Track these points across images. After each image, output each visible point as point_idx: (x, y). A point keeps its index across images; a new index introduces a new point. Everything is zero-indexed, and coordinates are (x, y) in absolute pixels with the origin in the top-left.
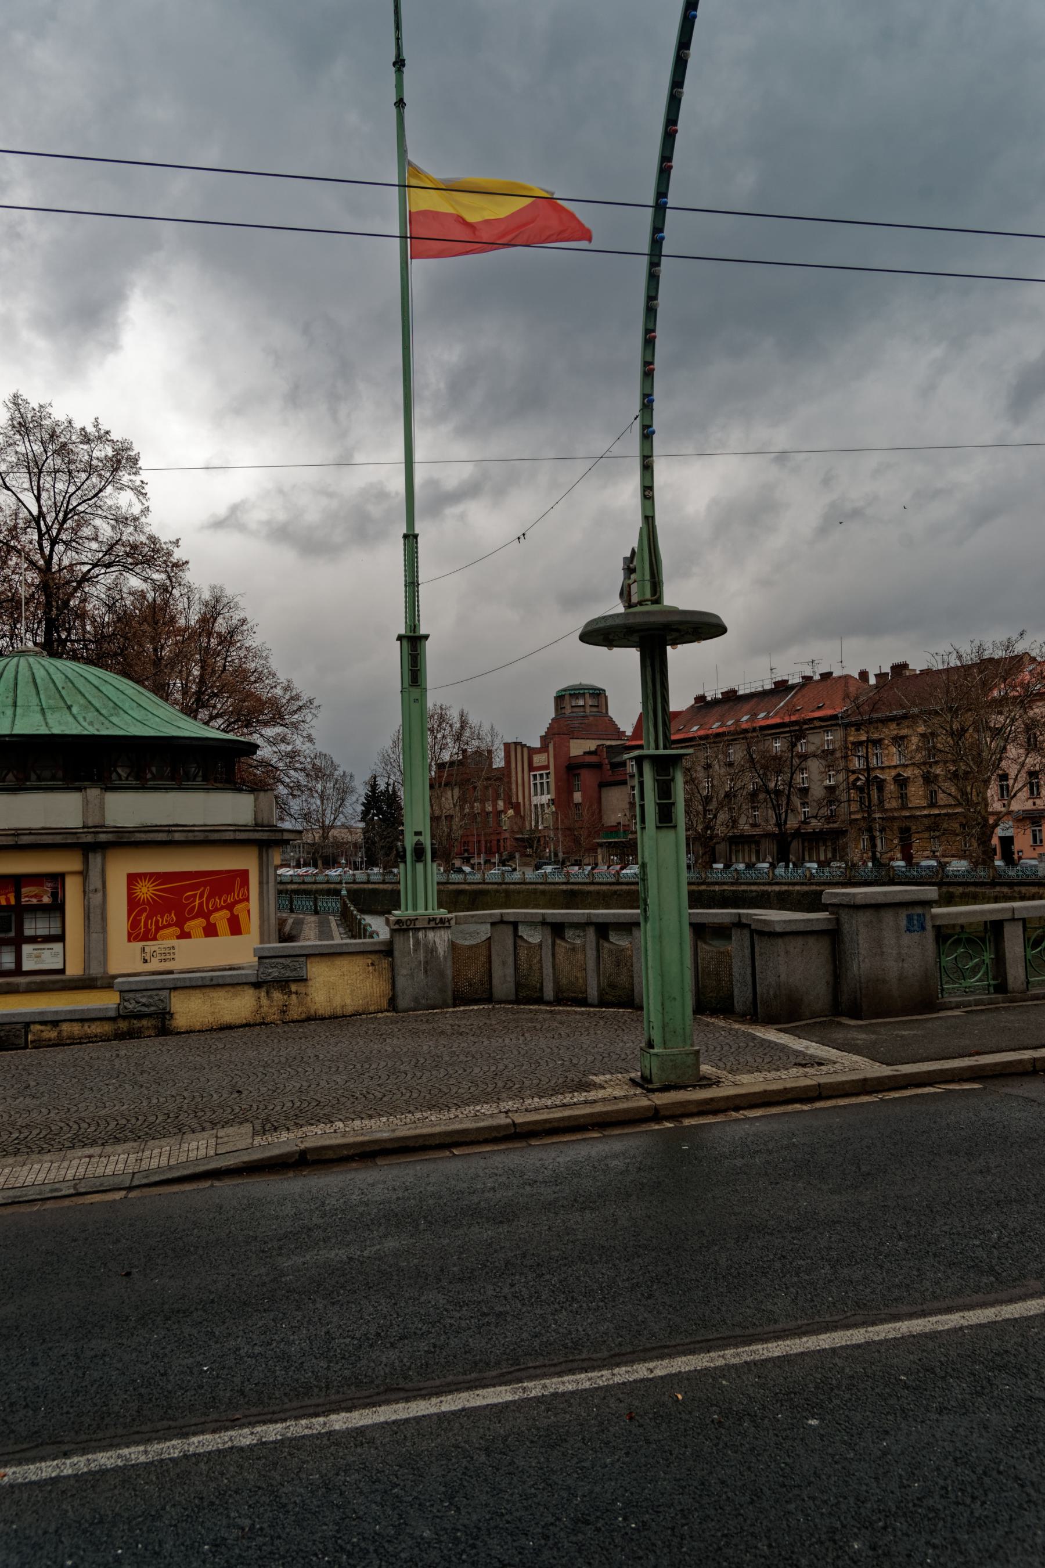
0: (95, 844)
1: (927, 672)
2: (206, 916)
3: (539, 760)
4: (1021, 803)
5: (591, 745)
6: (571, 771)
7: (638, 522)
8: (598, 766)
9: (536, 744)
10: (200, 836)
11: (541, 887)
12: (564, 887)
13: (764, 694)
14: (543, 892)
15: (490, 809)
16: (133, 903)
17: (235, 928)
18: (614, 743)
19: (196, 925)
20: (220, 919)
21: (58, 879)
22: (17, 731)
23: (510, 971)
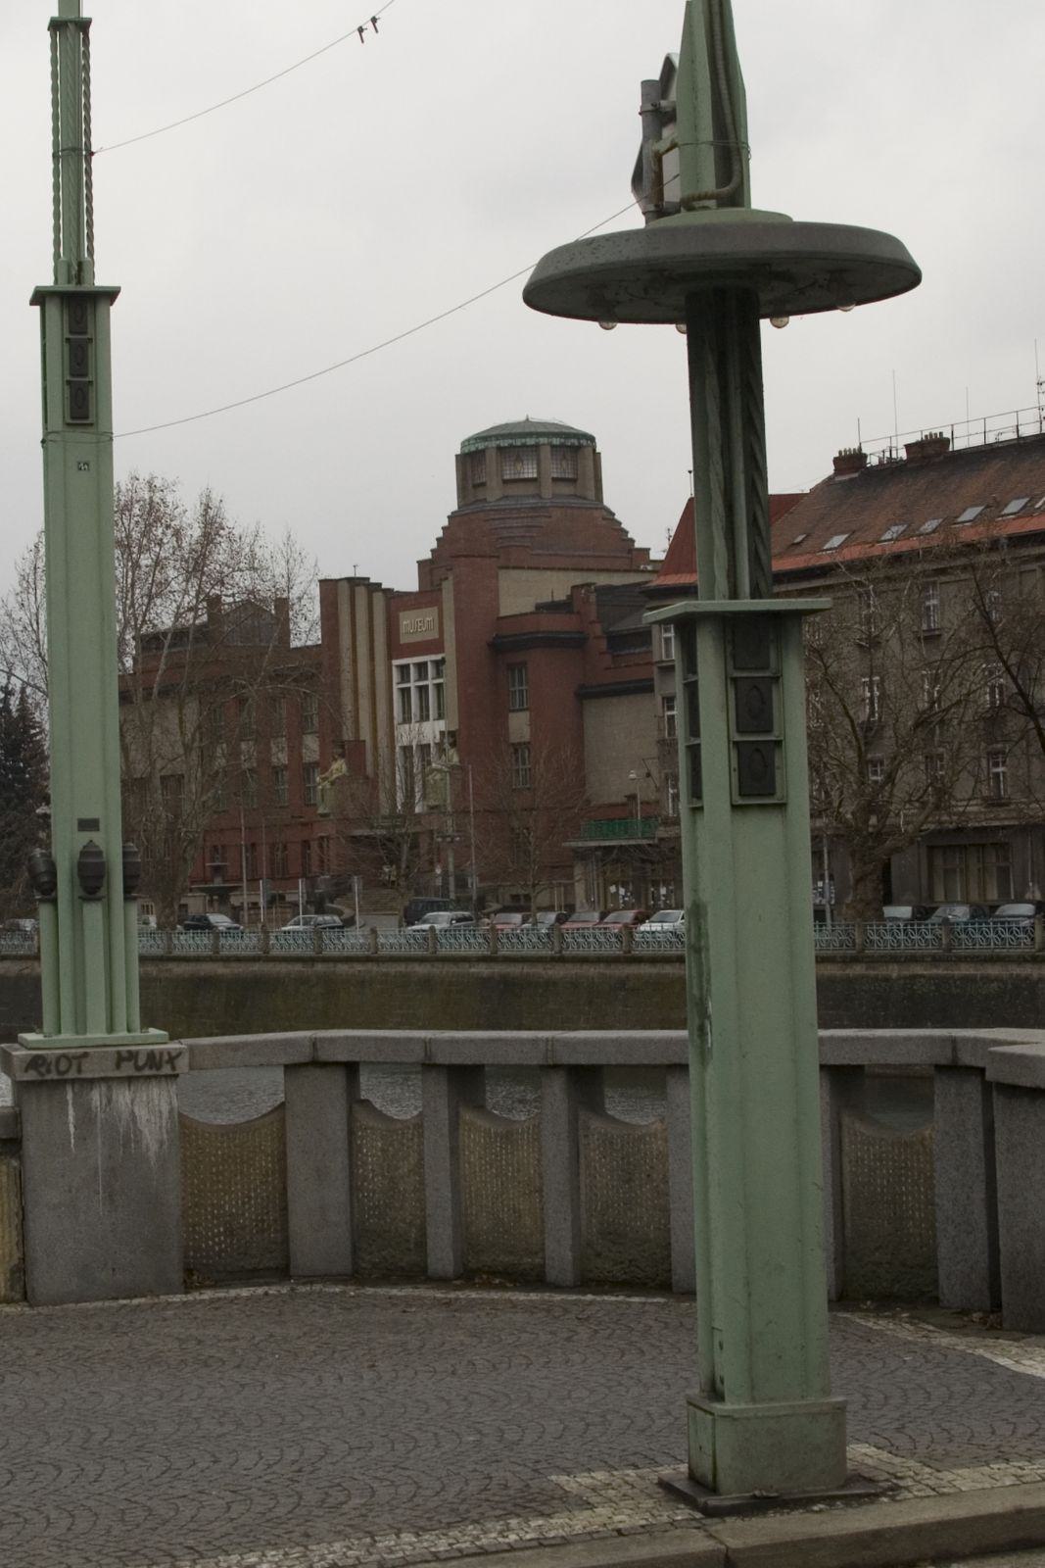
3: (415, 625)
5: (557, 586)
6: (502, 654)
8: (576, 643)
11: (420, 969)
12: (483, 970)
14: (426, 983)
15: (281, 757)
18: (617, 580)
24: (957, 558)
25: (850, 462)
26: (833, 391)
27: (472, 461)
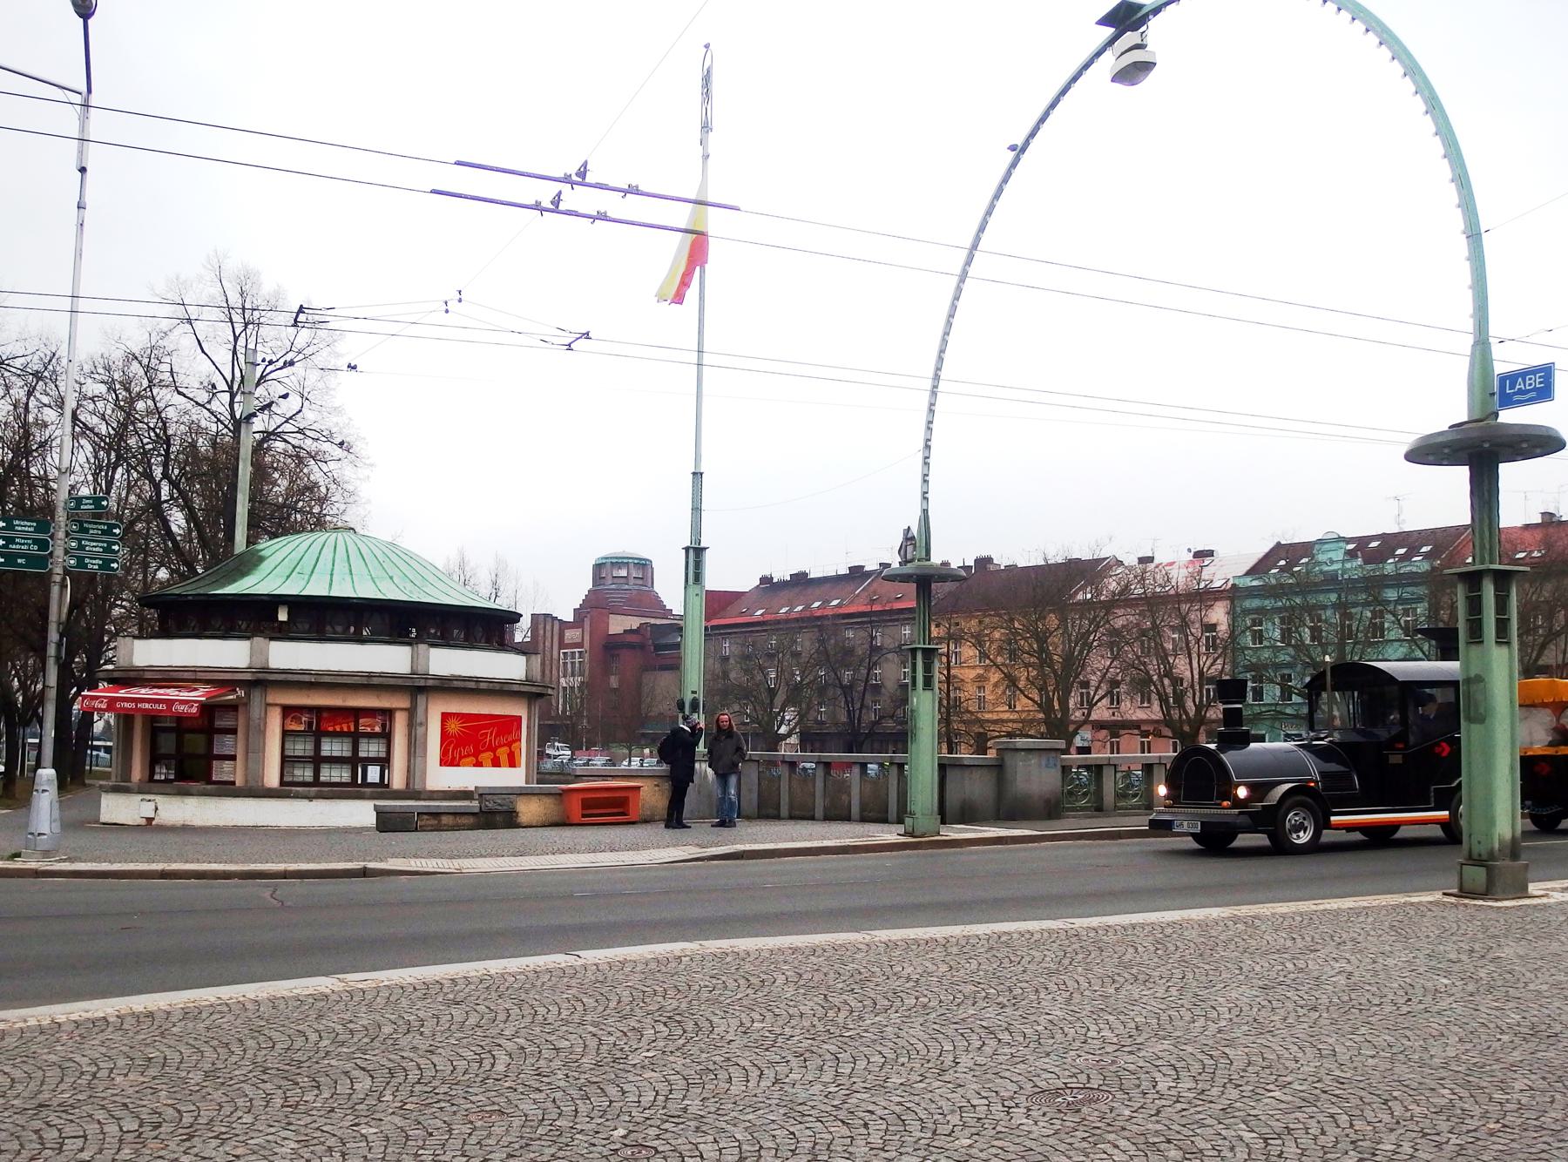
0: (419, 687)
1: (1011, 569)
2: (494, 750)
3: (571, 635)
4: (1101, 712)
5: (634, 623)
6: (611, 648)
7: (919, 513)
8: (642, 647)
9: (569, 617)
10: (498, 687)
13: (838, 579)
16: (445, 735)
17: (512, 763)
18: (658, 622)
19: (486, 756)
20: (503, 753)
21: (388, 714)
22: (304, 593)
23: (755, 796)
24: (809, 621)
25: (766, 580)
26: (1526, 493)
27: (598, 567)
